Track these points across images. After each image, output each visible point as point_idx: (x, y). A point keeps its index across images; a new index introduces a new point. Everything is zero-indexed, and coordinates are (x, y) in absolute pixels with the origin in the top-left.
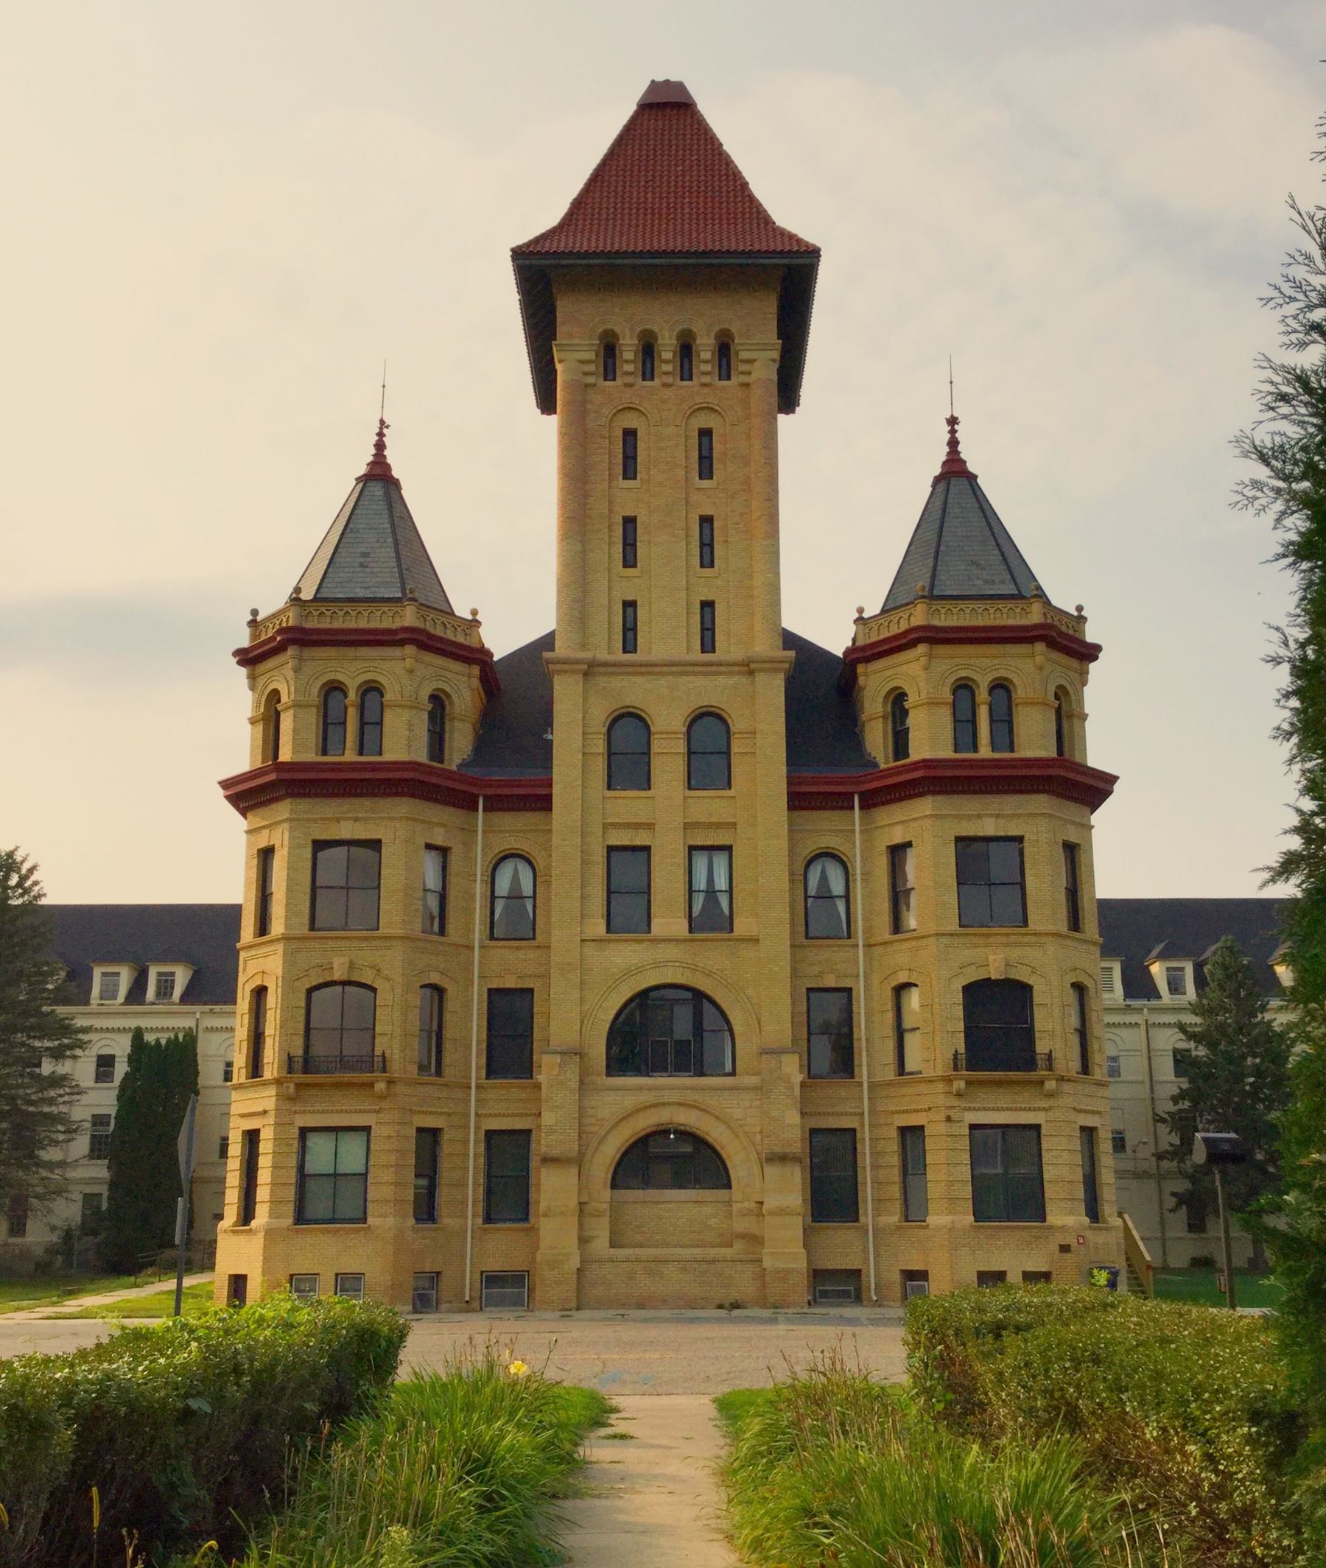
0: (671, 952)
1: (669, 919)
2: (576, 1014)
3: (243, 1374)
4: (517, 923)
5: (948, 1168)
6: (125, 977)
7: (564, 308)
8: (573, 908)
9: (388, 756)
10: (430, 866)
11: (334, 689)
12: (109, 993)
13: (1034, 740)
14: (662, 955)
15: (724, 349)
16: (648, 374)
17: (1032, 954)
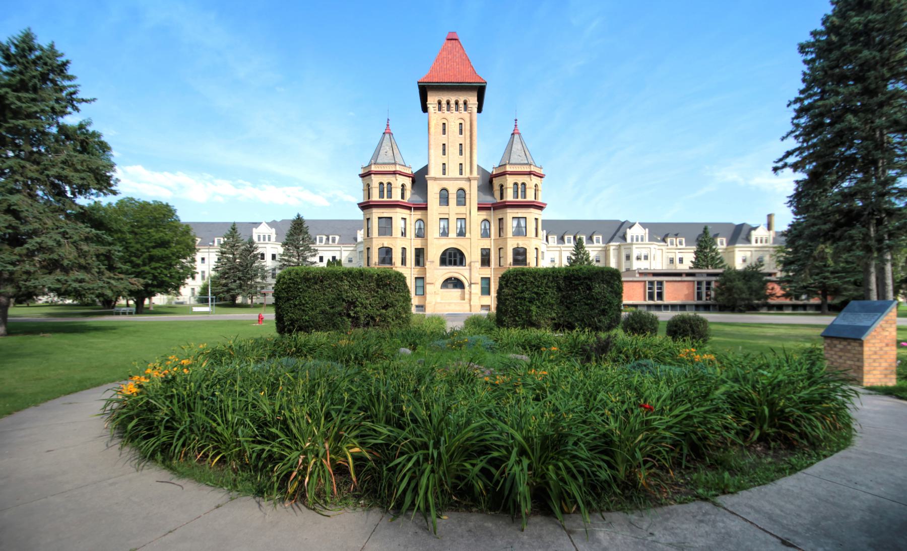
0: (453, 241)
1: (453, 234)
2: (434, 254)
3: (760, 439)
4: (421, 234)
5: (397, 257)
6: (324, 238)
7: (429, 94)
8: (433, 231)
9: (393, 199)
10: (403, 222)
11: (381, 184)
12: (321, 241)
13: (530, 197)
14: (452, 242)
15: (465, 103)
16: (448, 110)
17: (527, 242)
